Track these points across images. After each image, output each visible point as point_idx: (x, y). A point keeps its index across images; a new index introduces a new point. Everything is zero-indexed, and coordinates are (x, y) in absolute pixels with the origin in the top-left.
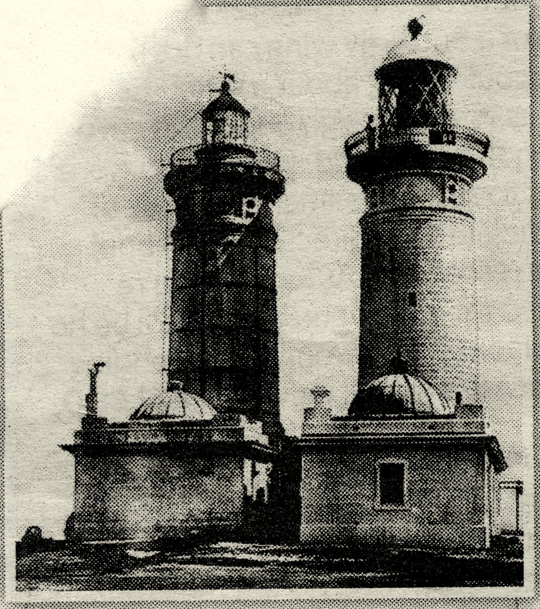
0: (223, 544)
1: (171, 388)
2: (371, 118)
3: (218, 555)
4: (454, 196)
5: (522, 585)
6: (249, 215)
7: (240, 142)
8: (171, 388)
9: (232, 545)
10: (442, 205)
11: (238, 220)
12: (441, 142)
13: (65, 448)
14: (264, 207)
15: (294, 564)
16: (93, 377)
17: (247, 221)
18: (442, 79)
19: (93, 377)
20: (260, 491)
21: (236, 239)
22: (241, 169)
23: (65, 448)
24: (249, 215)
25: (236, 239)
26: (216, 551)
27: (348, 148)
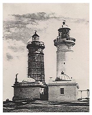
0: (37, 101)
1: (28, 77)
2: (58, 37)
3: (36, 103)
4: (70, 48)
5: (3, 3)
6: (39, 51)
7: (38, 41)
8: (28, 77)
9: (38, 101)
10: (68, 49)
11: (38, 52)
12: (68, 40)
13: (12, 86)
14: (42, 50)
15: (48, 104)
16: (16, 75)
17: (40, 52)
18: (68, 31)
19: (16, 75)
20: (42, 93)
21: (38, 55)
22: (38, 45)
23: (12, 86)
24: (39, 51)
25: (38, 55)
26: (36, 102)
27: (54, 41)
